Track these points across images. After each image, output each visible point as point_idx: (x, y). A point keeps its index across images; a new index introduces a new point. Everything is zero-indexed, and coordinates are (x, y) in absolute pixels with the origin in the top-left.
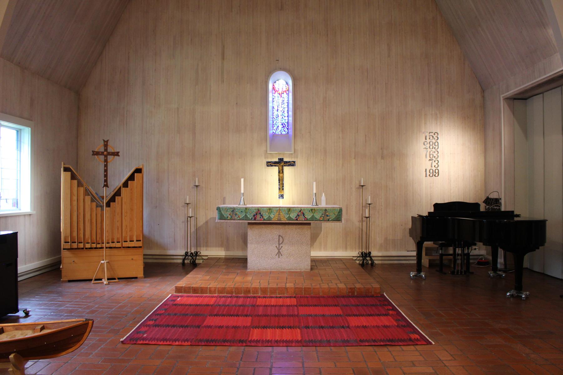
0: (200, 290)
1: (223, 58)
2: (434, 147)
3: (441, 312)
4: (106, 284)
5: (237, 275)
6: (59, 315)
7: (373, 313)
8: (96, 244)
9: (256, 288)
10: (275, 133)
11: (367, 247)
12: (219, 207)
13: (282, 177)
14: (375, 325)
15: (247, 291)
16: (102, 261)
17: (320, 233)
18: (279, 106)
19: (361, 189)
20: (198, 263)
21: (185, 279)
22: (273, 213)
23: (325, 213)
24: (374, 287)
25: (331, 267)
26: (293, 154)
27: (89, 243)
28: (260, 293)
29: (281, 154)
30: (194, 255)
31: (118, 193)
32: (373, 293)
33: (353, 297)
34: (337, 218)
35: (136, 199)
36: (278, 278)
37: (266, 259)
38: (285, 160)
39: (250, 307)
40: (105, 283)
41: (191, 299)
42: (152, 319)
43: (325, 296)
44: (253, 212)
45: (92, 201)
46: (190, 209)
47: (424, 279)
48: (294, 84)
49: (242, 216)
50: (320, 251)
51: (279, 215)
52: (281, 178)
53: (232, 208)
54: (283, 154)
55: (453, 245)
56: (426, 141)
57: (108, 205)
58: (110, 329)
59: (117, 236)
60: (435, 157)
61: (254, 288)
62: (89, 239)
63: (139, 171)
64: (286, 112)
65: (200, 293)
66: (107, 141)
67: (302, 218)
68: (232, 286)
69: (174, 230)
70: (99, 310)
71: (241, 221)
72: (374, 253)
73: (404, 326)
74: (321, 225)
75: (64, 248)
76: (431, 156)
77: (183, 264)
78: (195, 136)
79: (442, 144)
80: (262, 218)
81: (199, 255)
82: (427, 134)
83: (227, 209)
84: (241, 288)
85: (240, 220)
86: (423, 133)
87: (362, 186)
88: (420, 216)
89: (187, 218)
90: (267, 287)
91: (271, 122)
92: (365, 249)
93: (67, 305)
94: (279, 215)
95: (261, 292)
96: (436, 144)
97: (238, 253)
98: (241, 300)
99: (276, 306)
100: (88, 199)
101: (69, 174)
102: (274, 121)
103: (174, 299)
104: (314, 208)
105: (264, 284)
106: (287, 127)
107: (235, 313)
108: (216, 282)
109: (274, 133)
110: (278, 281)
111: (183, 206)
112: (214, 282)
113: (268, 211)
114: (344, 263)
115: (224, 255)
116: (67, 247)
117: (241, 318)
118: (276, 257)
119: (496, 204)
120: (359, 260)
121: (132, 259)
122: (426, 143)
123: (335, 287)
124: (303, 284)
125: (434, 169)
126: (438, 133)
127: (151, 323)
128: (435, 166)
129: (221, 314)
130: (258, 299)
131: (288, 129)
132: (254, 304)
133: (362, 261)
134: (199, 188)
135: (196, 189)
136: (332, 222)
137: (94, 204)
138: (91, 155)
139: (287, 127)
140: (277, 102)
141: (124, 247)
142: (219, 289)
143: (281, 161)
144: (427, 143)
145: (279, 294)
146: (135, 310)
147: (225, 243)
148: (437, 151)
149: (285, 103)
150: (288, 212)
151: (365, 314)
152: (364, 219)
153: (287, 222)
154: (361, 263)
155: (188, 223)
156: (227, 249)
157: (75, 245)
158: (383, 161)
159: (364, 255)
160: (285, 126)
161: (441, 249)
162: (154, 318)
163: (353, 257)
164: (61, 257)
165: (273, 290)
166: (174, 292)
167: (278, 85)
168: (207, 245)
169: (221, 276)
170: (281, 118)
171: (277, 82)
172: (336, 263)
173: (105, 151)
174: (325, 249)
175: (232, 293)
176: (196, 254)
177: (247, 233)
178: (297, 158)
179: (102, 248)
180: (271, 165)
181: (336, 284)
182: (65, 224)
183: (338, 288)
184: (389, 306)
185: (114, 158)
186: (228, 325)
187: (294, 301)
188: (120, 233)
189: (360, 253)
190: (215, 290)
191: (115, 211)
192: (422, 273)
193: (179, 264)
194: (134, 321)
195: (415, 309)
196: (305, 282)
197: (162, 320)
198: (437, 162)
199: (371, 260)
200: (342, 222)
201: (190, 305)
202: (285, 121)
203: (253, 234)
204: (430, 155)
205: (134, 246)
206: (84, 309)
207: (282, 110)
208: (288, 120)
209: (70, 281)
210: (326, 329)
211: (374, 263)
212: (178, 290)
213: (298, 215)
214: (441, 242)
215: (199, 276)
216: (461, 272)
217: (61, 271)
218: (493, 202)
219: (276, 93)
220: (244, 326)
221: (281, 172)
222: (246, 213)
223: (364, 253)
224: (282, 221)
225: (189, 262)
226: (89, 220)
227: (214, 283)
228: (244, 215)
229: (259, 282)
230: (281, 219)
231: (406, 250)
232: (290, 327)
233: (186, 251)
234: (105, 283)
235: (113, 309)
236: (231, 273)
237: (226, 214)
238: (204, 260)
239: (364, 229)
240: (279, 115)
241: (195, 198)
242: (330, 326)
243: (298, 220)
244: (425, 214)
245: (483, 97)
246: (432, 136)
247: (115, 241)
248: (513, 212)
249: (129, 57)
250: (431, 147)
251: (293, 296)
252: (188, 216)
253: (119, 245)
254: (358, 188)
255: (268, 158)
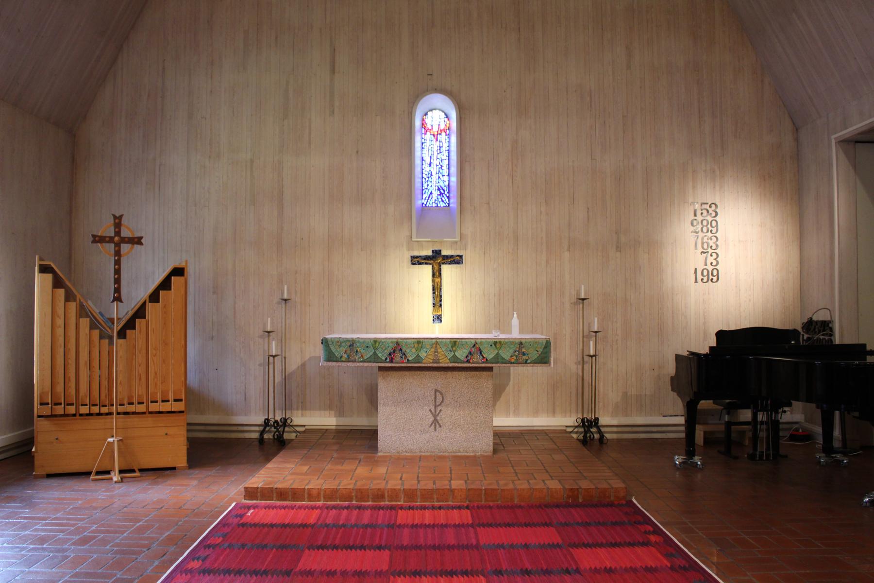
0: (290, 493)
1: (333, 71)
2: (710, 229)
3: (746, 537)
4: (116, 482)
5: (359, 463)
6: (18, 547)
7: (619, 540)
8: (98, 407)
9: (395, 489)
10: (426, 205)
11: (593, 410)
12: (326, 339)
13: (439, 284)
14: (629, 566)
15: (379, 495)
16: (109, 438)
17: (508, 384)
18: (432, 156)
19: (581, 305)
20: (287, 439)
21: (263, 471)
22: (424, 349)
23: (520, 349)
24: (614, 486)
25: (530, 448)
26: (459, 243)
27: (86, 405)
28: (402, 500)
29: (437, 242)
30: (280, 424)
31: (140, 313)
32: (612, 498)
33: (577, 505)
34: (542, 359)
35: (174, 324)
36: (435, 470)
37: (411, 433)
38: (444, 253)
39: (386, 529)
40: (115, 479)
41: (272, 512)
42: (197, 556)
43: (522, 504)
44: (388, 347)
45: (93, 326)
46: (274, 342)
47: (700, 469)
48: (461, 118)
49: (368, 354)
50: (507, 417)
51: (435, 352)
52: (437, 285)
53: (349, 341)
54: (441, 242)
55: (752, 406)
56: (695, 218)
57: (122, 334)
58: (115, 578)
59: (138, 392)
60: (711, 247)
61: (391, 489)
62: (86, 397)
63: (178, 272)
64: (445, 167)
65: (290, 499)
66: (121, 217)
67: (477, 357)
68: (351, 487)
69: (245, 379)
70: (96, 537)
71: (366, 364)
72: (603, 421)
73: (684, 569)
74: (509, 370)
75: (39, 414)
76: (705, 246)
77: (261, 440)
78: (282, 211)
79: (725, 224)
80: (405, 358)
81: (289, 425)
82: (697, 206)
83: (340, 342)
84: (368, 489)
85: (365, 362)
86: (691, 205)
87: (583, 299)
88: (692, 353)
89: (269, 358)
90: (415, 488)
91: (418, 184)
92: (588, 413)
93: (37, 527)
94: (435, 352)
95: (404, 497)
96: (714, 223)
97: (360, 421)
98: (368, 513)
99: (434, 526)
100: (85, 323)
101: (49, 277)
102: (424, 183)
103: (239, 512)
104: (500, 340)
105: (410, 483)
106: (448, 195)
107: (358, 542)
108: (321, 476)
109: (424, 205)
110: (436, 475)
111: (261, 337)
112: (317, 477)
113: (416, 346)
114: (551, 439)
115: (335, 424)
116: (44, 413)
117: (369, 553)
118: (430, 429)
119: (824, 330)
120: (576, 433)
121: (166, 434)
122: (695, 223)
123: (543, 487)
124: (482, 481)
125: (710, 268)
126: (716, 205)
127: (195, 564)
128: (711, 264)
129: (331, 544)
130: (400, 511)
131: (448, 197)
132: (393, 522)
133: (583, 435)
134: (289, 304)
135: (284, 305)
136: (532, 365)
137: (96, 333)
138: (90, 243)
139: (448, 195)
140: (430, 148)
141: (151, 413)
142: (325, 491)
143: (437, 255)
144: (698, 223)
145: (439, 502)
146: (166, 535)
147: (337, 405)
148: (715, 236)
149: (444, 151)
150: (452, 347)
151: (604, 542)
152: (586, 359)
153: (451, 365)
154: (581, 437)
155: (270, 366)
156: (340, 413)
157: (59, 410)
158: (618, 254)
159: (587, 424)
160: (444, 193)
161: (728, 413)
162: (203, 554)
163: (566, 426)
164: (33, 430)
165: (427, 494)
166: (243, 496)
167: (432, 119)
168: (304, 407)
169: (329, 466)
170: (437, 178)
171: (429, 113)
172: (538, 439)
173: (115, 236)
174: (517, 413)
175: (350, 498)
176: (285, 422)
177: (377, 385)
178: (466, 250)
179: (110, 414)
180: (418, 261)
181: (543, 481)
182: (41, 370)
183: (548, 489)
184: (646, 525)
185: (132, 248)
186: (346, 570)
187: (466, 516)
188: (144, 386)
189: (579, 421)
190: (319, 494)
191: (134, 347)
192: (696, 458)
193: (253, 442)
194: (162, 559)
195: (697, 531)
196: (486, 478)
197: (216, 560)
198: (714, 256)
199: (600, 432)
200: (550, 366)
201: (272, 526)
202: (444, 182)
203: (387, 387)
204: (703, 243)
205: (170, 410)
206: (69, 534)
207: (438, 164)
208: (449, 181)
209: (50, 476)
210: (535, 576)
211: (605, 438)
212: (251, 493)
213: (470, 353)
214: (728, 401)
215: (288, 466)
216: (768, 456)
217: (34, 457)
218: (817, 327)
219: (428, 133)
220: (377, 570)
221: (437, 274)
222: (375, 348)
223: (586, 419)
224: (441, 363)
225: (271, 437)
226: (86, 362)
227: (317, 479)
228: (371, 354)
229: (399, 477)
230: (439, 359)
231: (662, 414)
232: (465, 573)
233: (267, 417)
234: (115, 479)
235: (125, 534)
236: (347, 459)
237: (338, 352)
238: (299, 434)
239: (587, 377)
240: (434, 173)
241: (282, 323)
242: (542, 569)
243: (471, 361)
244: (704, 350)
245: (797, 140)
246: (705, 209)
247: (135, 400)
248: (864, 345)
249: (164, 68)
250: (705, 229)
251: (463, 505)
252: (270, 354)
253: (142, 408)
254: (575, 304)
255: (413, 250)
